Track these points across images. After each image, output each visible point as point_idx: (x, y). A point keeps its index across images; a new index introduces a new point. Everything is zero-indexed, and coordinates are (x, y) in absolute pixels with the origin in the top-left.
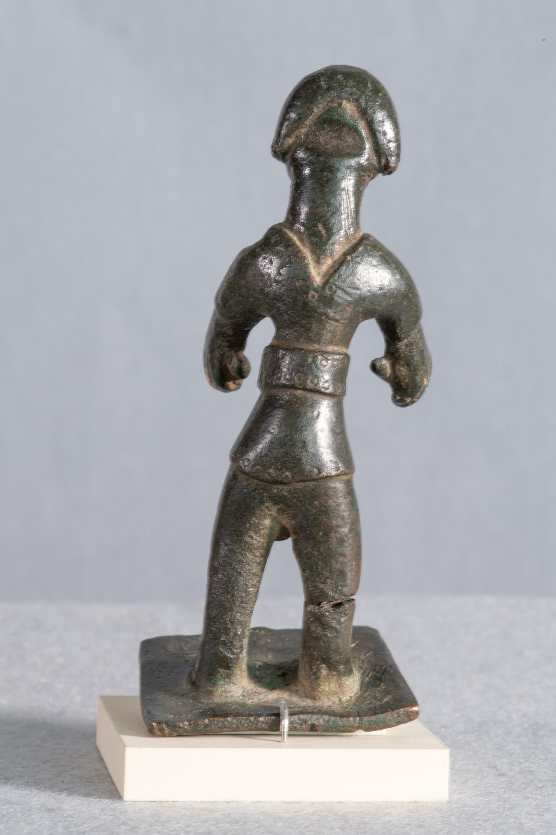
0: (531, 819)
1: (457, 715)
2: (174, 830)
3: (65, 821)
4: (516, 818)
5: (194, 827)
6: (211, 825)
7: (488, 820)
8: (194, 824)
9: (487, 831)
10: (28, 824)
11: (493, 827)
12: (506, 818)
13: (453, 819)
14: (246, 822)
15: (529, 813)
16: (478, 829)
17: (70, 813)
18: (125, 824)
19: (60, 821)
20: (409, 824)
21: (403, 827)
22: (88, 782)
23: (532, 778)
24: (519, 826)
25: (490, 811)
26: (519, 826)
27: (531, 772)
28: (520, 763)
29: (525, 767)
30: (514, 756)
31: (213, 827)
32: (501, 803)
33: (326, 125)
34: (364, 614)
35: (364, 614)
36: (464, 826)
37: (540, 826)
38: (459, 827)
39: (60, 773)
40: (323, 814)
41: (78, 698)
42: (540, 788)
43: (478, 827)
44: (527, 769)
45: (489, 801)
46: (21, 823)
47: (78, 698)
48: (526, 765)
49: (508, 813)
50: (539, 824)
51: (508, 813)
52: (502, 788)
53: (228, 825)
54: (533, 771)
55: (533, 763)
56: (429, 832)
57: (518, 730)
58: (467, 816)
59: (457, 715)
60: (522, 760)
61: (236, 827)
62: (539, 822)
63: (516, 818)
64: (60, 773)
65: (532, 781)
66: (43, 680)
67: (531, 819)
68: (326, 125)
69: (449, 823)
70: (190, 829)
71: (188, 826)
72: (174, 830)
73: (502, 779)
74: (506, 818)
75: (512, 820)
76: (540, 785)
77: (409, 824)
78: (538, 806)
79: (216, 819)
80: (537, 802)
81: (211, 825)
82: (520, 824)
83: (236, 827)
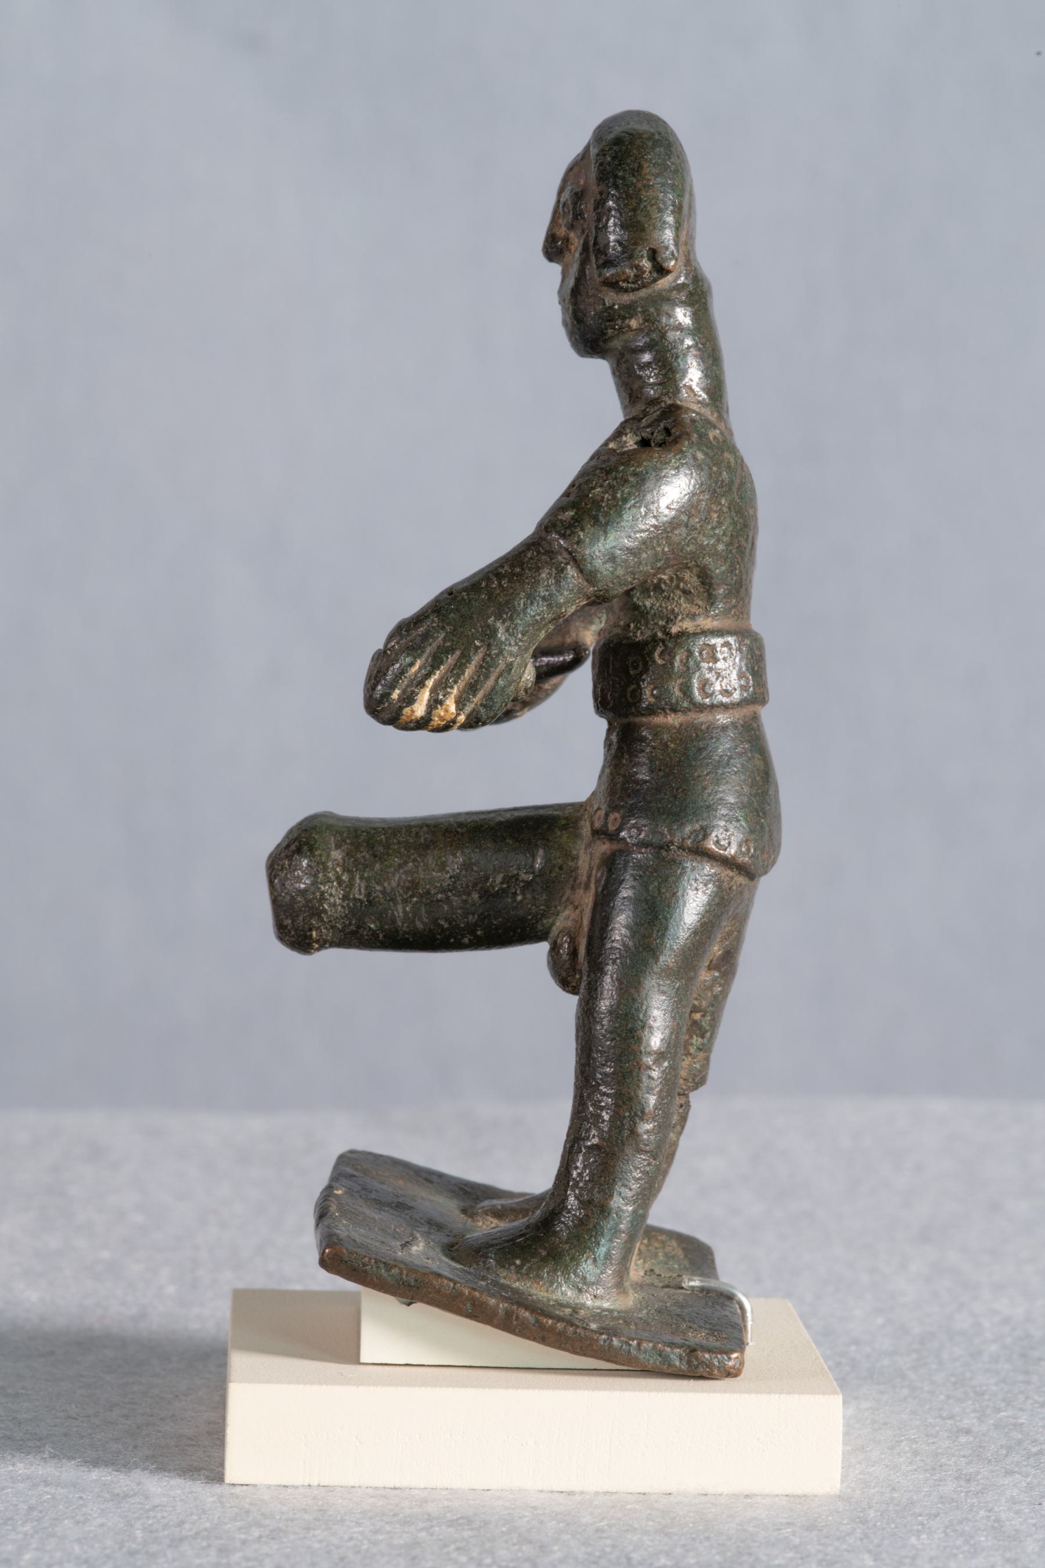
0: (1017, 1512)
1: (880, 1321)
2: (351, 1539)
3: (148, 1518)
4: (990, 1511)
5: (388, 1533)
6: (422, 1529)
7: (936, 1515)
8: (388, 1528)
9: (936, 1536)
10: (78, 1522)
11: (947, 1527)
12: (971, 1510)
13: (872, 1514)
14: (486, 1523)
15: (1013, 1501)
16: (918, 1531)
17: (157, 1501)
18: (258, 1524)
19: (139, 1518)
20: (789, 1524)
21: (779, 1530)
22: (193, 1445)
23: (1020, 1436)
24: (996, 1525)
25: (941, 1498)
26: (996, 1525)
27: (1019, 1427)
28: (998, 1410)
29: (1008, 1417)
30: (986, 1397)
31: (423, 1534)
32: (962, 1483)
33: (614, 217)
34: (574, 999)
35: (574, 999)
36: (893, 1526)
37: (1034, 1525)
38: (883, 1529)
39: (138, 1428)
40: (629, 1507)
41: (171, 1290)
42: (1036, 1454)
43: (920, 1527)
44: (1011, 1421)
45: (940, 1480)
46: (66, 1522)
47: (171, 1290)
48: (1010, 1413)
49: (974, 1501)
50: (1034, 1521)
51: (974, 1501)
52: (964, 1456)
53: (451, 1530)
54: (1023, 1424)
55: (1021, 1410)
56: (827, 1537)
57: (994, 1348)
58: (898, 1508)
59: (880, 1321)
60: (1003, 1405)
61: (467, 1534)
62: (1032, 1518)
63: (990, 1511)
64: (138, 1428)
65: (1020, 1443)
66: (105, 1255)
67: (1017, 1512)
68: (614, 217)
69: (864, 1522)
70: (381, 1537)
71: (376, 1532)
72: (351, 1539)
73: (963, 1439)
74: (971, 1510)
75: (982, 1513)
76: (1034, 1450)
77: (789, 1524)
78: (1030, 1487)
79: (430, 1518)
80: (1029, 1479)
81: (422, 1529)
82: (997, 1521)
83: (467, 1534)
